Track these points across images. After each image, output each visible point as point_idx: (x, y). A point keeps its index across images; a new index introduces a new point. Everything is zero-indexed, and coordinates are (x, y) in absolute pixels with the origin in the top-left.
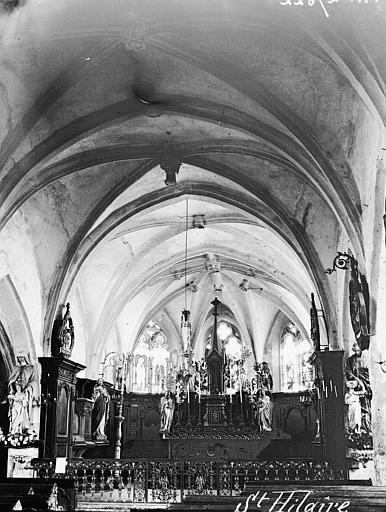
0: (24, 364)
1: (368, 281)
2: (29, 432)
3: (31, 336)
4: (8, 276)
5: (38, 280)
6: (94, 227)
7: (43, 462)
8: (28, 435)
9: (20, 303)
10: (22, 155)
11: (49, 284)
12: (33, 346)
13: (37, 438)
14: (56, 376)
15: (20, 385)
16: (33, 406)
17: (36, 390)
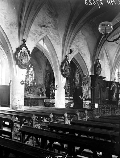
0: (86, 77)
1: (101, 65)
2: (88, 96)
3: (87, 69)
4: (79, 53)
5: (89, 53)
6: (102, 38)
7: (92, 105)
8: (87, 97)
9: (83, 60)
10: (76, 17)
11: (92, 54)
12: (88, 72)
13: (90, 98)
14: (95, 80)
15: (85, 83)
16: (89, 89)
17: (90, 84)
